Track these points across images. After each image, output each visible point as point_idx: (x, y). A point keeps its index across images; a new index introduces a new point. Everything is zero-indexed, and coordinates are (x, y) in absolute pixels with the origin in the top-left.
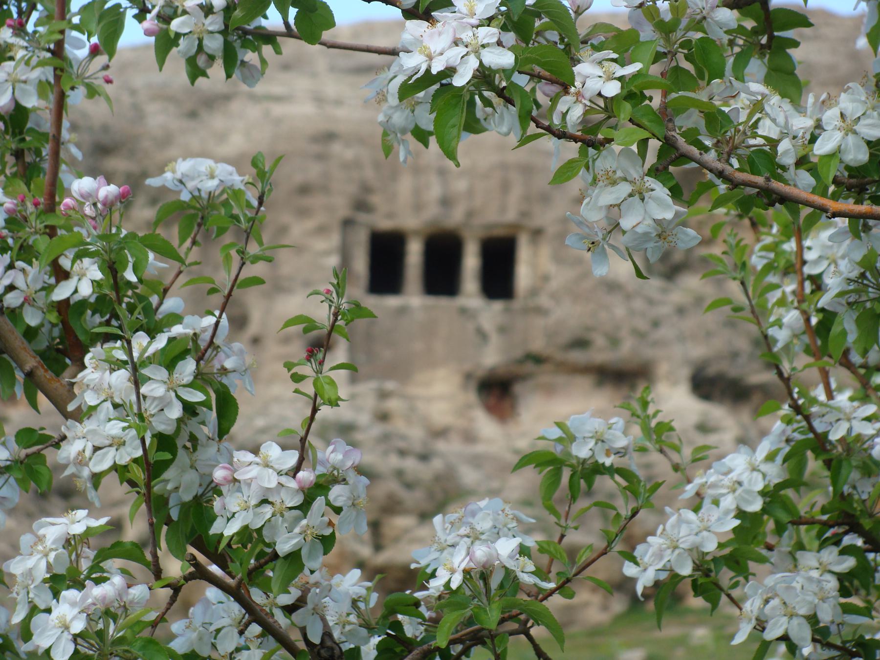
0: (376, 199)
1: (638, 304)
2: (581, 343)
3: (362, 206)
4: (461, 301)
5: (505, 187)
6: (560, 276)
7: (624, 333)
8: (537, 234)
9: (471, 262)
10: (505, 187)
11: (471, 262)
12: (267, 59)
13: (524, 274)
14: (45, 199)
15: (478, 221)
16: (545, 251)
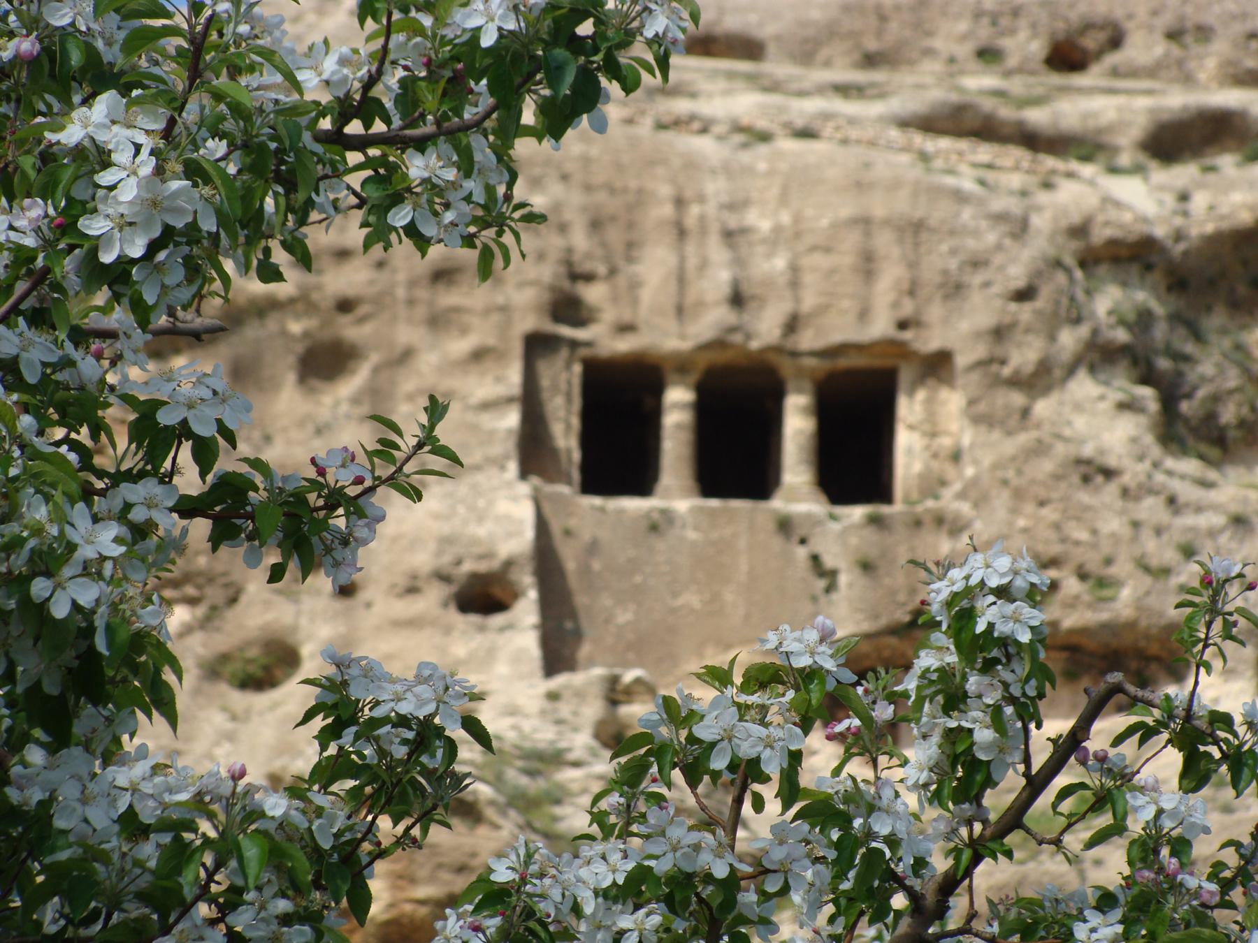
0: (593, 294)
1: (1152, 509)
3: (567, 308)
4: (777, 503)
5: (868, 265)
6: (986, 451)
7: (1122, 568)
8: (938, 366)
9: (797, 423)
10: (868, 265)
11: (797, 423)
12: (770, 903)
13: (908, 447)
14: (1142, 288)
15: (807, 340)
16: (952, 401)
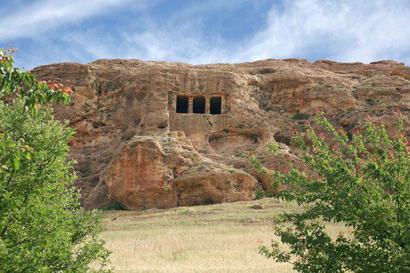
2: (241, 127)
